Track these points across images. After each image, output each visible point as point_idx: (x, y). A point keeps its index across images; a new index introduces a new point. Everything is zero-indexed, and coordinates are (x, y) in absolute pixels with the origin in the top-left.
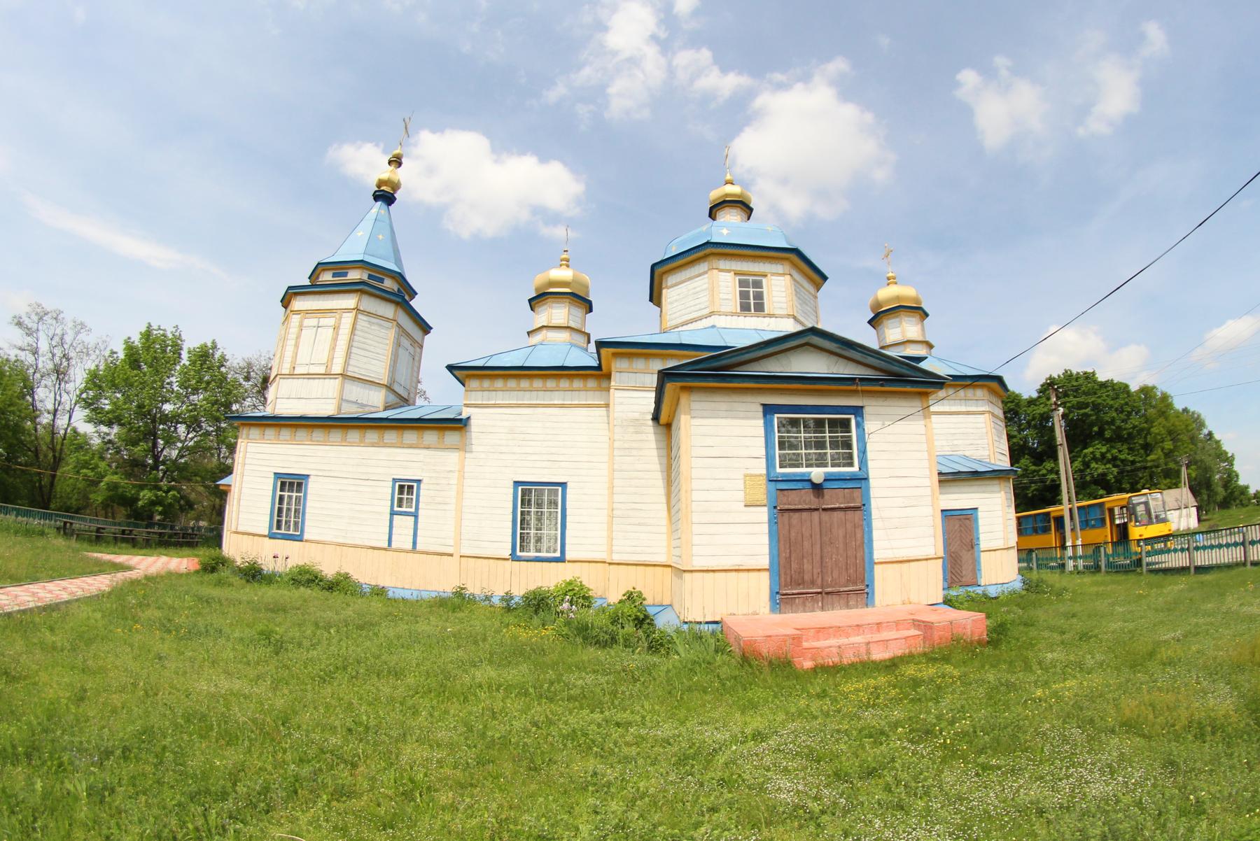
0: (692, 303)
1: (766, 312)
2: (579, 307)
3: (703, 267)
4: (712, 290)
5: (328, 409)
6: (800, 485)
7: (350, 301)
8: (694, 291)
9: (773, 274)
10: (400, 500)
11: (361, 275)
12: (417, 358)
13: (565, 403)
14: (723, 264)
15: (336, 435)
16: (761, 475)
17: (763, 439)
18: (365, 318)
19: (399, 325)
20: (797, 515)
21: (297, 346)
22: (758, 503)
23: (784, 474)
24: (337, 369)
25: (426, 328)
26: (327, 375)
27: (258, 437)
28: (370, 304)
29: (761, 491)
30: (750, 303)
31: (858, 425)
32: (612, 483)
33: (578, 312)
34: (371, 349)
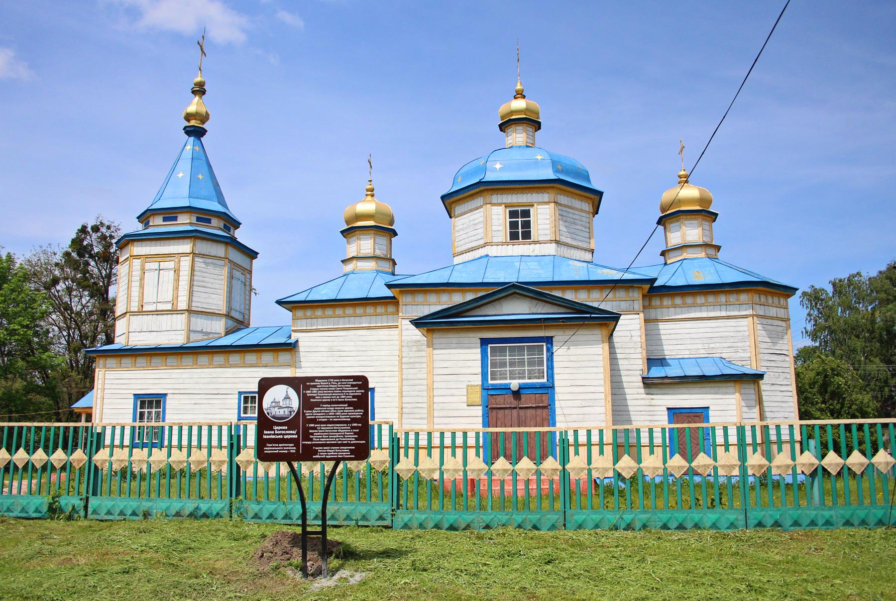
0: (472, 233)
1: (532, 240)
2: (384, 236)
3: (479, 201)
4: (487, 222)
5: (178, 340)
6: (504, 392)
7: (185, 247)
8: (473, 222)
9: (540, 203)
10: (246, 408)
11: (190, 219)
12: (248, 283)
13: (371, 325)
14: (495, 198)
15: (188, 360)
16: (477, 386)
17: (480, 361)
18: (201, 260)
19: (230, 261)
20: (502, 411)
21: (142, 286)
22: (475, 404)
23: (492, 385)
24: (183, 305)
26: (174, 311)
27: (115, 366)
28: (204, 247)
29: (477, 397)
30: (518, 232)
31: (548, 350)
32: (402, 389)
33: (382, 240)
34: (210, 285)
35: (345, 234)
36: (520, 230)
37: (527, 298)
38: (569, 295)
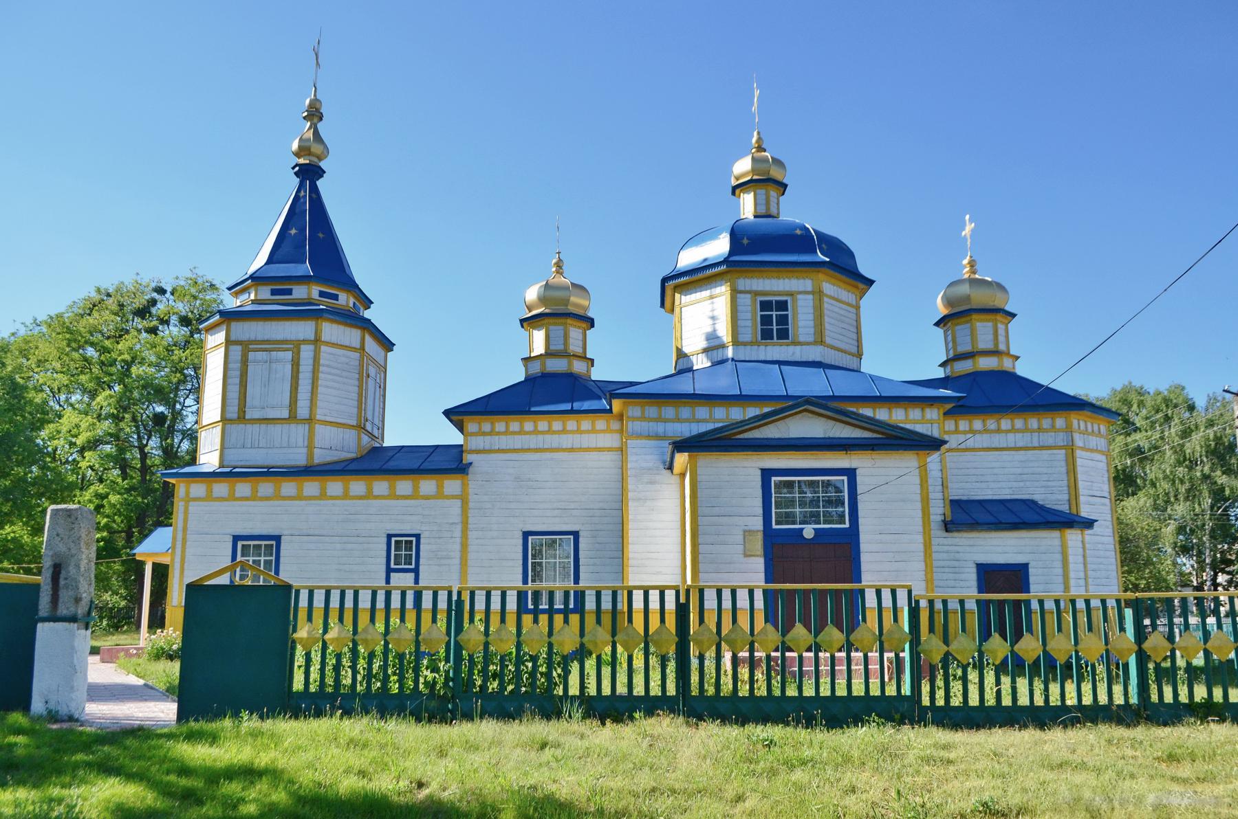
16: (758, 531)
25: (388, 345)
26: (293, 417)
29: (758, 544)
30: (773, 329)
35: (525, 324)
36: (775, 327)
37: (820, 418)
38: (882, 414)
